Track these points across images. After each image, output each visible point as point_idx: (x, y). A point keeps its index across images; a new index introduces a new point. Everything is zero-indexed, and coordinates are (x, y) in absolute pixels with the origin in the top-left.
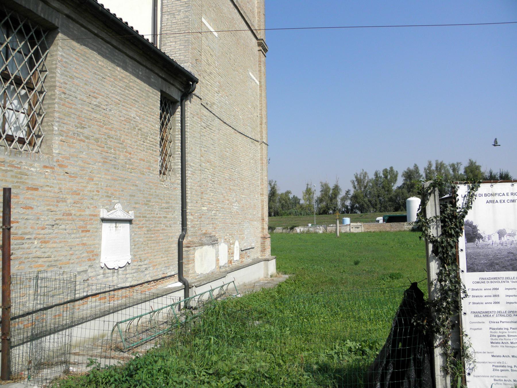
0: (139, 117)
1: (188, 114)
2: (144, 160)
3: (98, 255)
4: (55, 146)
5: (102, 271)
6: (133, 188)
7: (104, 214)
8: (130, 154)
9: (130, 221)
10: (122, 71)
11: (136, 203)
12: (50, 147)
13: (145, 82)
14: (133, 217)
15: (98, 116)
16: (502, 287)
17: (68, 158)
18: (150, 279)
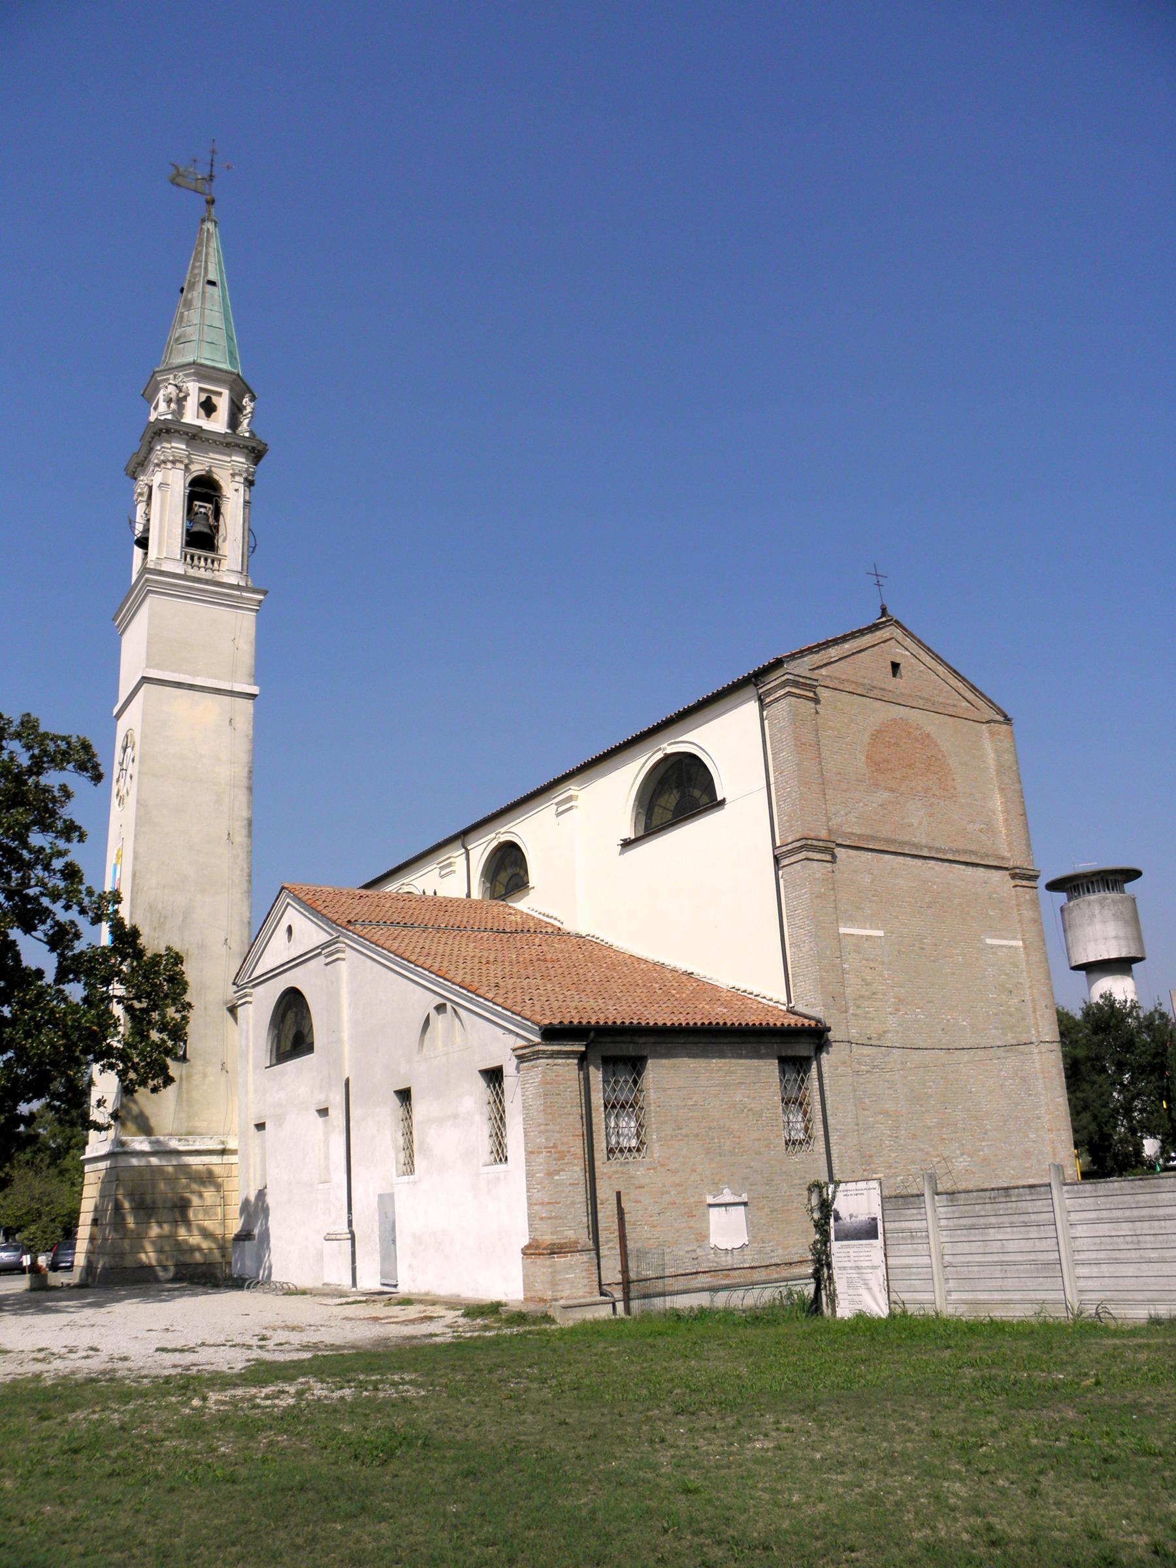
0: (748, 1097)
1: (825, 1069)
2: (759, 1140)
3: (707, 1237)
4: (655, 1151)
5: (712, 1251)
6: (748, 1170)
7: (710, 1200)
8: (739, 1137)
9: (745, 1204)
10: (719, 1061)
11: (751, 1185)
12: (652, 1152)
13: (752, 1058)
14: (746, 1200)
15: (696, 1114)
16: (851, 1250)
17: (668, 1158)
18: (779, 1262)
